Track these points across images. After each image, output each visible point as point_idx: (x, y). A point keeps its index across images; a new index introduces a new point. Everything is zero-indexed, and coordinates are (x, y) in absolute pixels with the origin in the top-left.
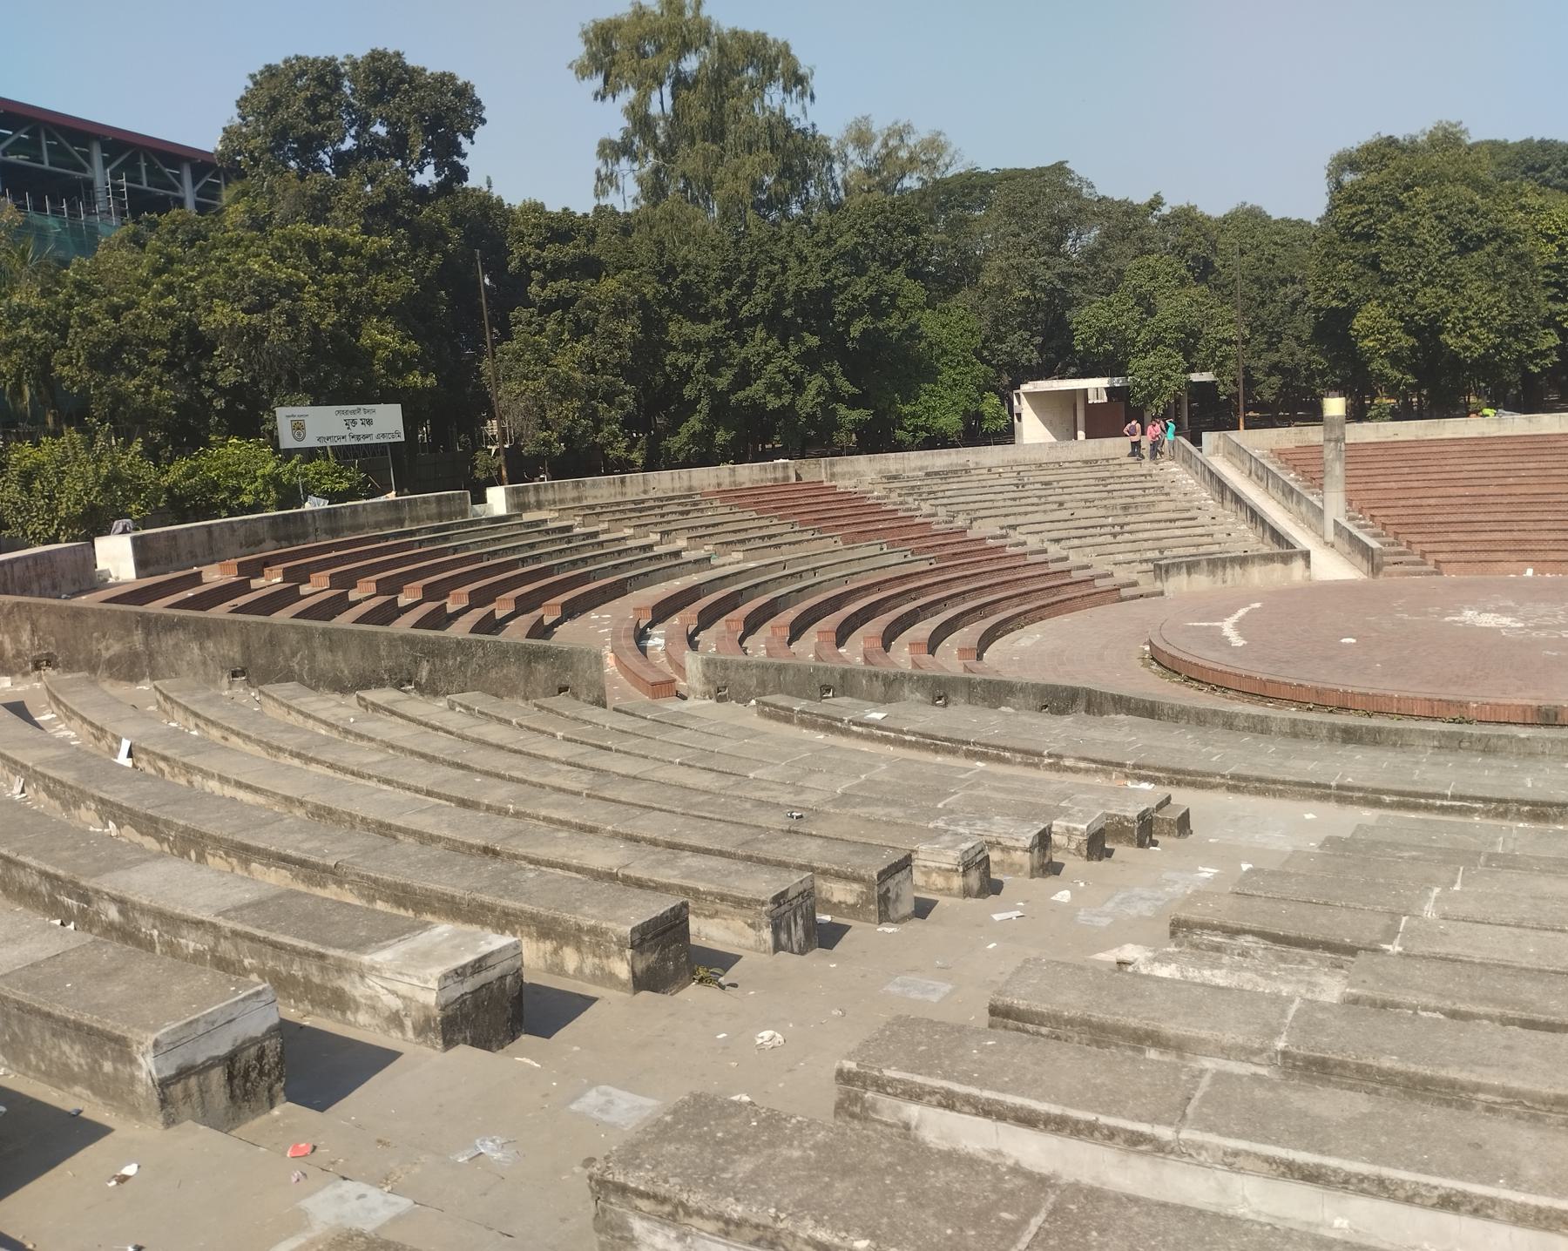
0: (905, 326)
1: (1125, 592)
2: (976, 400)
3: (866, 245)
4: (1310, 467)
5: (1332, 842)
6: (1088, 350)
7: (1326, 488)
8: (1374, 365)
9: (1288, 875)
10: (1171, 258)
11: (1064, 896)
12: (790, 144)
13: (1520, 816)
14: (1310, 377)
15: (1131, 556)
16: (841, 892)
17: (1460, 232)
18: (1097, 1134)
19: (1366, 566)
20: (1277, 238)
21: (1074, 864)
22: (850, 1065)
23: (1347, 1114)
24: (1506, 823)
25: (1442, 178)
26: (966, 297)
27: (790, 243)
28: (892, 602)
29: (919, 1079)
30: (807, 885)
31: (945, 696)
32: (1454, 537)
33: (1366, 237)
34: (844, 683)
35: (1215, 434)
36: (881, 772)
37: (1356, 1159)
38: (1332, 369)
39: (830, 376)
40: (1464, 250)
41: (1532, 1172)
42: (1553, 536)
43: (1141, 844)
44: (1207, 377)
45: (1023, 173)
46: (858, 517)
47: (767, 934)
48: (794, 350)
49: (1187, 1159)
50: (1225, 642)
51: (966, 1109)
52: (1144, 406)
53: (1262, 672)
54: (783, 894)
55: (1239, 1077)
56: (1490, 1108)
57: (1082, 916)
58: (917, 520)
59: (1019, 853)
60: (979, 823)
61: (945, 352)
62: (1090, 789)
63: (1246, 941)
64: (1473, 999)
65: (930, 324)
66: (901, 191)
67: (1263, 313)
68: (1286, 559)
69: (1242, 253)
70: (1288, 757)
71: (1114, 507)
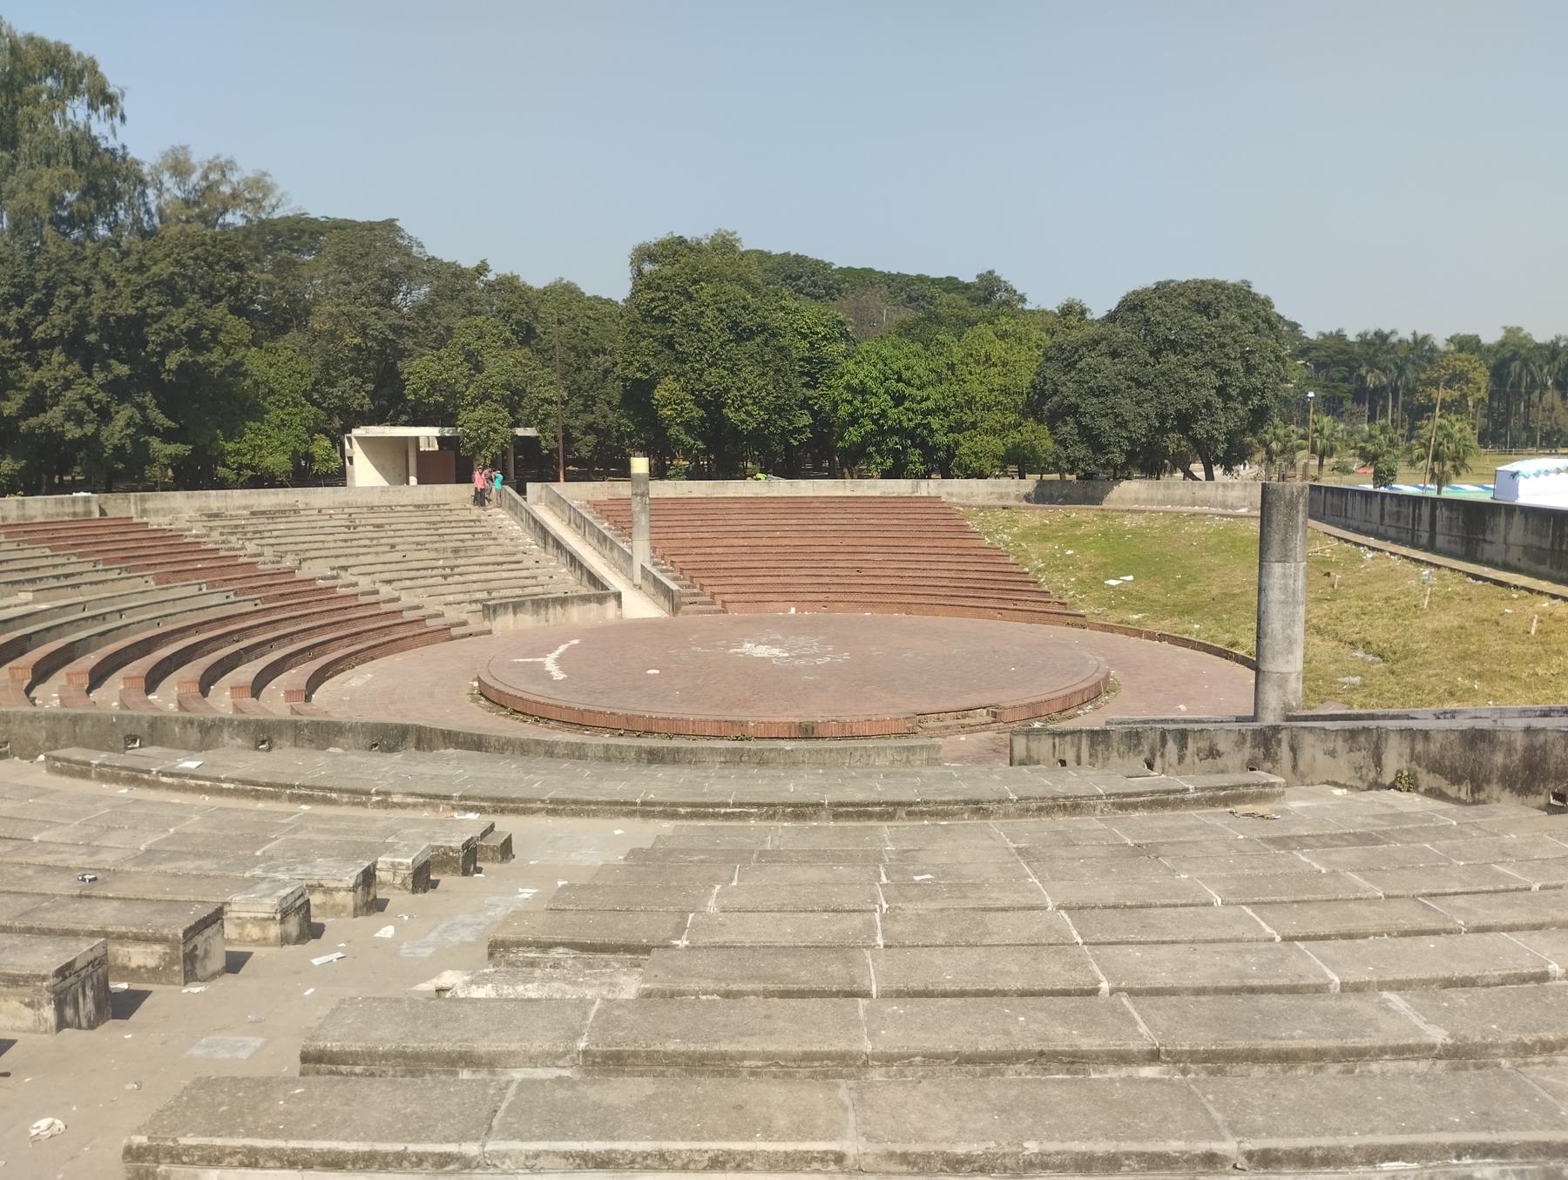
0: (228, 362)
1: (455, 631)
2: (305, 442)
3: (184, 276)
4: (620, 516)
5: (636, 854)
6: (419, 400)
7: (635, 536)
8: (672, 431)
9: (596, 887)
10: (497, 321)
11: (387, 932)
12: (96, 162)
13: (785, 816)
14: (621, 438)
15: (461, 597)
16: (140, 956)
17: (736, 324)
18: (405, 1163)
19: (667, 605)
20: (590, 313)
21: (399, 899)
22: (141, 1140)
23: (635, 1099)
24: (775, 823)
25: (722, 278)
26: (293, 339)
27: (95, 265)
28: (211, 645)
29: (218, 1142)
30: (99, 952)
31: (270, 740)
32: (736, 580)
33: (663, 320)
34: (156, 732)
35: (539, 485)
36: (194, 824)
37: (641, 1139)
38: (638, 432)
39: (142, 408)
40: (740, 339)
41: (782, 1122)
42: (809, 580)
43: (466, 873)
44: (530, 432)
45: (353, 225)
46: (174, 556)
47: (49, 1012)
48: (99, 377)
49: (492, 1170)
50: (547, 676)
51: (271, 1164)
52: (473, 456)
53: (579, 702)
54: (69, 965)
55: (542, 1082)
56: (754, 1073)
57: (405, 949)
58: (241, 560)
59: (343, 893)
60: (300, 867)
61: (272, 392)
62: (417, 823)
63: (558, 953)
64: (742, 978)
65: (256, 362)
66: (223, 226)
67: (580, 378)
68: (601, 600)
69: (560, 322)
70: (600, 779)
71: (445, 550)
